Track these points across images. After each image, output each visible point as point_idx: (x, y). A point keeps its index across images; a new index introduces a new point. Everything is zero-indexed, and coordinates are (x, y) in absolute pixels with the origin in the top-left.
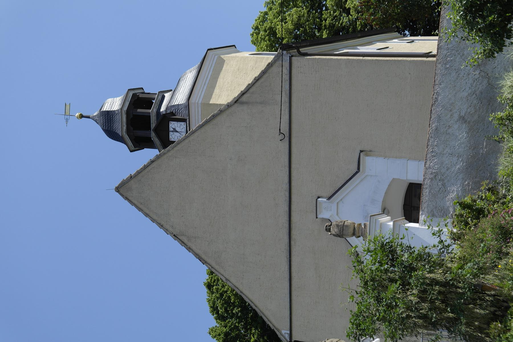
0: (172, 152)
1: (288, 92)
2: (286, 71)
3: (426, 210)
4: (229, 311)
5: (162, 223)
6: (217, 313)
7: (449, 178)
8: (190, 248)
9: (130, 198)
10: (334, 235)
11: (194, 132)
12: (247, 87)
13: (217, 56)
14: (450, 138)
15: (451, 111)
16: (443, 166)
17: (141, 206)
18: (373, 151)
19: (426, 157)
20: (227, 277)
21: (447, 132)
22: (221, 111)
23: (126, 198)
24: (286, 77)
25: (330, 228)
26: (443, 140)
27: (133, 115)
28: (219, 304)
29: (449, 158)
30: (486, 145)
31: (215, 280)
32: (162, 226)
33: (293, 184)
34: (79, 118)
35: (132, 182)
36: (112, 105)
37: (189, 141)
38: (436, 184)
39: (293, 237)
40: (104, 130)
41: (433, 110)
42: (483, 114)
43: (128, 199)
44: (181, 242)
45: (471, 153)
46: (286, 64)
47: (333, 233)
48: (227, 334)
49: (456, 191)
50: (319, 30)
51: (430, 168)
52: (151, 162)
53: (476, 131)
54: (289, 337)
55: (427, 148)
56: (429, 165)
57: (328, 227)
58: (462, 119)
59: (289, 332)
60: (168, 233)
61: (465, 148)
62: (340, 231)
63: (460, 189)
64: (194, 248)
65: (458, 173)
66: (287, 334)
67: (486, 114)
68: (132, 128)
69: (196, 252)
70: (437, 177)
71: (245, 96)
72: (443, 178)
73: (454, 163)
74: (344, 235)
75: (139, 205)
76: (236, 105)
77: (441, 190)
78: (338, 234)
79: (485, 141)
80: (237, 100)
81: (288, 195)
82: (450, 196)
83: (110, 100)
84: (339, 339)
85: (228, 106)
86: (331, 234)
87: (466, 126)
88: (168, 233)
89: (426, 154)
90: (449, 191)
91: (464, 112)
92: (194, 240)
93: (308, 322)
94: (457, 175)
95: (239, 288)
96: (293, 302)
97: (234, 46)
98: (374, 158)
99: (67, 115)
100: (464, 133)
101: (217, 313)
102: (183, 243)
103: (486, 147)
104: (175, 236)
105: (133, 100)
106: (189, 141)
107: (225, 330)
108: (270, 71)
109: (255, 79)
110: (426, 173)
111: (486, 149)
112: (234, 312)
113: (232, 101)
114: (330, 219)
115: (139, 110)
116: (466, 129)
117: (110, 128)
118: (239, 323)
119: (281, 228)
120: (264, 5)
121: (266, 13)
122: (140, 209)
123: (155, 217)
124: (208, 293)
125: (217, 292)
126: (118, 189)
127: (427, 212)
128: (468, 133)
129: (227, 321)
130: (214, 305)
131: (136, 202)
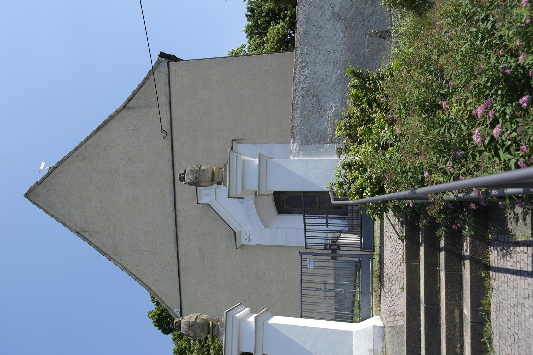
3: (298, 136)
5: (66, 222)
7: (324, 91)
9: (38, 203)
12: (132, 93)
14: (322, 41)
15: (321, 8)
16: (317, 77)
17: (48, 209)
18: (244, 140)
19: (295, 70)
21: (319, 35)
22: (111, 117)
23: (35, 203)
25: (185, 176)
26: (314, 46)
29: (323, 67)
30: (368, 45)
32: (66, 225)
35: (39, 187)
37: (86, 146)
38: (309, 102)
39: (179, 223)
41: (299, 10)
42: (361, 6)
43: (36, 203)
44: (83, 237)
45: (350, 56)
48: (159, 315)
49: (335, 107)
51: (300, 82)
52: (54, 168)
53: (355, 28)
54: (180, 314)
55: (295, 59)
56: (299, 79)
57: (182, 175)
58: (337, 16)
59: (179, 310)
60: (72, 231)
61: (342, 51)
62: (196, 177)
63: (339, 104)
64: (94, 242)
65: (336, 84)
66: (179, 311)
67: (365, 5)
70: (309, 93)
71: (132, 101)
72: (317, 92)
73: (330, 73)
74: (201, 182)
75: (45, 208)
76: (124, 110)
77: (315, 109)
78: (193, 182)
79: (366, 39)
80: (125, 106)
81: (172, 187)
82: (327, 114)
84: (200, 314)
85: (117, 112)
86: (185, 183)
87: (342, 24)
89: (294, 66)
90: (325, 108)
91: (338, 7)
92: (94, 235)
93: (195, 300)
94: (334, 87)
95: (135, 274)
96: (182, 282)
98: (245, 145)
100: (340, 33)
102: (85, 239)
103: (368, 47)
104: (78, 233)
106: (86, 146)
107: (158, 312)
109: (139, 86)
110: (295, 90)
111: (369, 49)
113: (121, 107)
114: (210, 203)
116: (342, 27)
119: (169, 217)
122: (46, 212)
123: (60, 218)
126: (27, 195)
127: (300, 139)
128: (344, 33)
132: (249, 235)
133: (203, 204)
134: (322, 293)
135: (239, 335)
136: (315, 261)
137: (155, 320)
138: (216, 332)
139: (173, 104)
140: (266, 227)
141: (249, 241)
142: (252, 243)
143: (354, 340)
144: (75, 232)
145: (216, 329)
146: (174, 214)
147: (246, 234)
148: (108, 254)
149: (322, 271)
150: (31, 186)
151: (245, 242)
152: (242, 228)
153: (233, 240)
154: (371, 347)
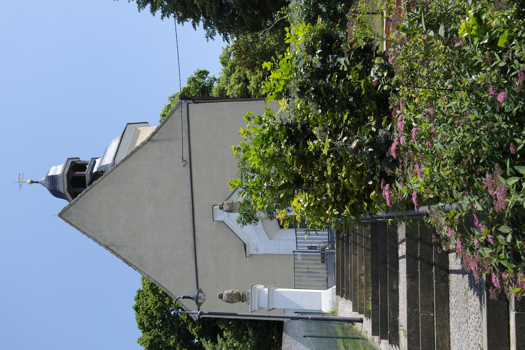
0: (102, 182)
1: (187, 130)
2: (185, 115)
4: (152, 324)
5: (96, 238)
6: (144, 327)
8: (118, 255)
9: (70, 221)
10: (226, 211)
11: (118, 166)
13: (134, 129)
17: (79, 227)
20: (149, 274)
23: (67, 221)
24: (185, 119)
28: (145, 319)
31: (141, 303)
33: (195, 197)
35: (71, 208)
36: (55, 171)
39: (197, 237)
40: (49, 190)
44: (111, 251)
46: (185, 110)
47: (225, 209)
64: (121, 254)
69: (123, 257)
71: (156, 135)
76: (149, 143)
80: (150, 139)
81: (191, 207)
83: (53, 168)
88: (101, 245)
97: (147, 123)
99: (21, 183)
101: (144, 327)
102: (113, 252)
104: (107, 247)
105: (72, 166)
107: (150, 337)
108: (173, 116)
112: (156, 323)
113: (146, 140)
115: (77, 173)
118: (160, 332)
120: (168, 100)
121: (170, 105)
122: (78, 229)
123: (90, 234)
124: (136, 314)
125: (143, 310)
126: (60, 215)
129: (151, 331)
130: (141, 321)
131: (75, 224)
132: (257, 246)
133: (218, 221)
134: (306, 274)
135: (259, 296)
136: (302, 255)
137: (147, 346)
138: (244, 299)
139: (192, 138)
140: (271, 239)
141: (257, 251)
142: (259, 253)
143: (323, 297)
144: (105, 246)
145: (244, 297)
146: (192, 230)
147: (254, 245)
148: (134, 265)
149: (307, 262)
150: (65, 207)
151: (254, 252)
152: (251, 240)
153: (244, 250)
154: (331, 299)
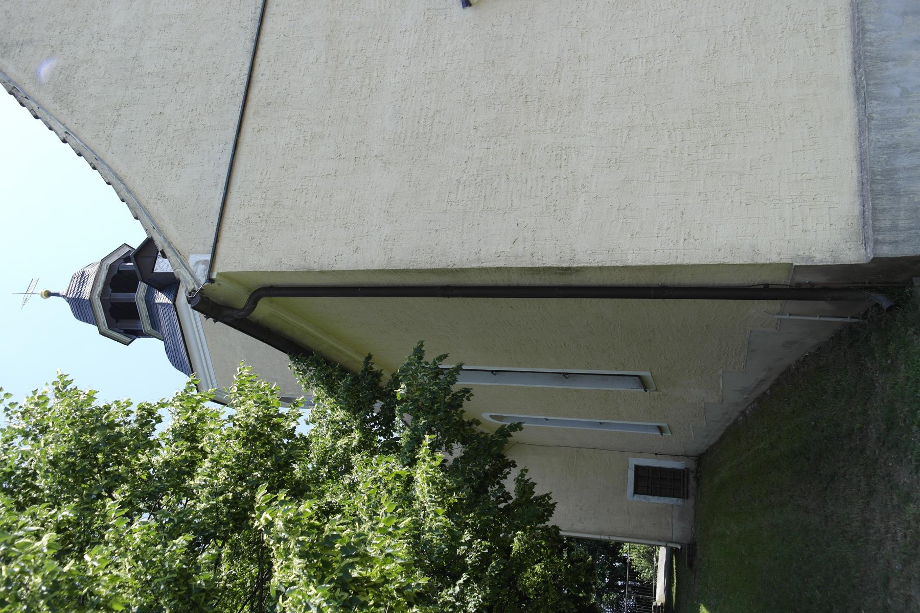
27: (119, 271)
34: (44, 296)
50: (589, 591)
68: (111, 290)
117: (79, 294)
